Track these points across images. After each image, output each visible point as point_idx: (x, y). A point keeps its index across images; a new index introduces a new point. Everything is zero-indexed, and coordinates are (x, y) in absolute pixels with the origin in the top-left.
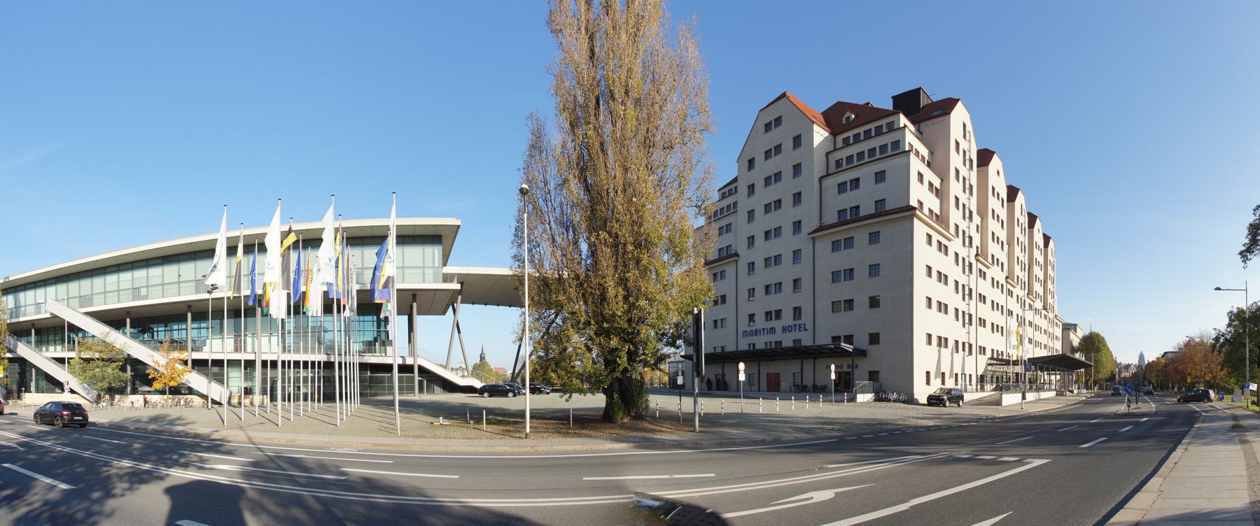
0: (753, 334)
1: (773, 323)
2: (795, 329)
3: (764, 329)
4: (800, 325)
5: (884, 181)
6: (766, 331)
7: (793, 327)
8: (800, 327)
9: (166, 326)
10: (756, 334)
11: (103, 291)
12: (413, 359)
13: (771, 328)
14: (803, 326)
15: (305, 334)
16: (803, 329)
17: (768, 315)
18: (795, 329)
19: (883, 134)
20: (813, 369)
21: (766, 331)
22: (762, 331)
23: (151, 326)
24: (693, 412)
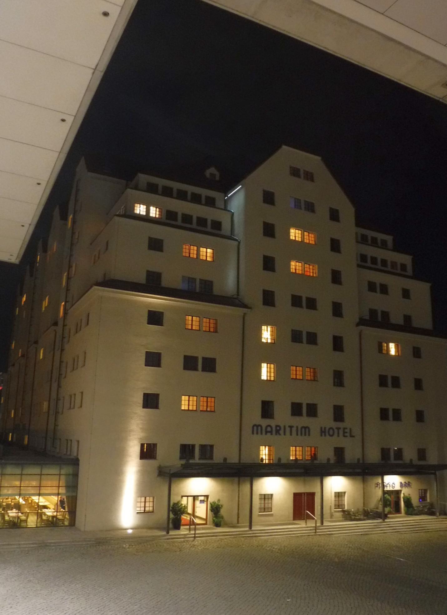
0: (271, 432)
1: (304, 421)
2: (338, 433)
3: (291, 427)
4: (344, 429)
5: (409, 290)
6: (294, 430)
7: (336, 431)
8: (344, 432)
9: (313, 376)
10: (278, 432)
11: (140, 501)
12: (212, 331)
13: (302, 427)
14: (348, 431)
15: (266, 510)
16: (348, 434)
17: (296, 410)
18: (338, 433)
19: (77, 496)
20: (242, 457)
21: (294, 430)
22: (288, 430)
23: (31, 496)
24: (193, 497)
